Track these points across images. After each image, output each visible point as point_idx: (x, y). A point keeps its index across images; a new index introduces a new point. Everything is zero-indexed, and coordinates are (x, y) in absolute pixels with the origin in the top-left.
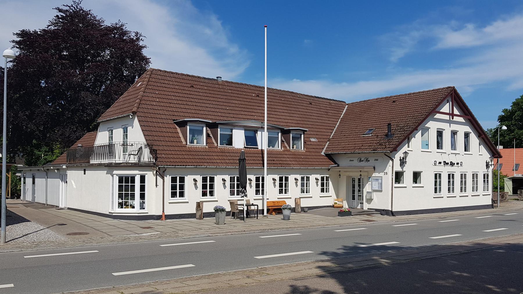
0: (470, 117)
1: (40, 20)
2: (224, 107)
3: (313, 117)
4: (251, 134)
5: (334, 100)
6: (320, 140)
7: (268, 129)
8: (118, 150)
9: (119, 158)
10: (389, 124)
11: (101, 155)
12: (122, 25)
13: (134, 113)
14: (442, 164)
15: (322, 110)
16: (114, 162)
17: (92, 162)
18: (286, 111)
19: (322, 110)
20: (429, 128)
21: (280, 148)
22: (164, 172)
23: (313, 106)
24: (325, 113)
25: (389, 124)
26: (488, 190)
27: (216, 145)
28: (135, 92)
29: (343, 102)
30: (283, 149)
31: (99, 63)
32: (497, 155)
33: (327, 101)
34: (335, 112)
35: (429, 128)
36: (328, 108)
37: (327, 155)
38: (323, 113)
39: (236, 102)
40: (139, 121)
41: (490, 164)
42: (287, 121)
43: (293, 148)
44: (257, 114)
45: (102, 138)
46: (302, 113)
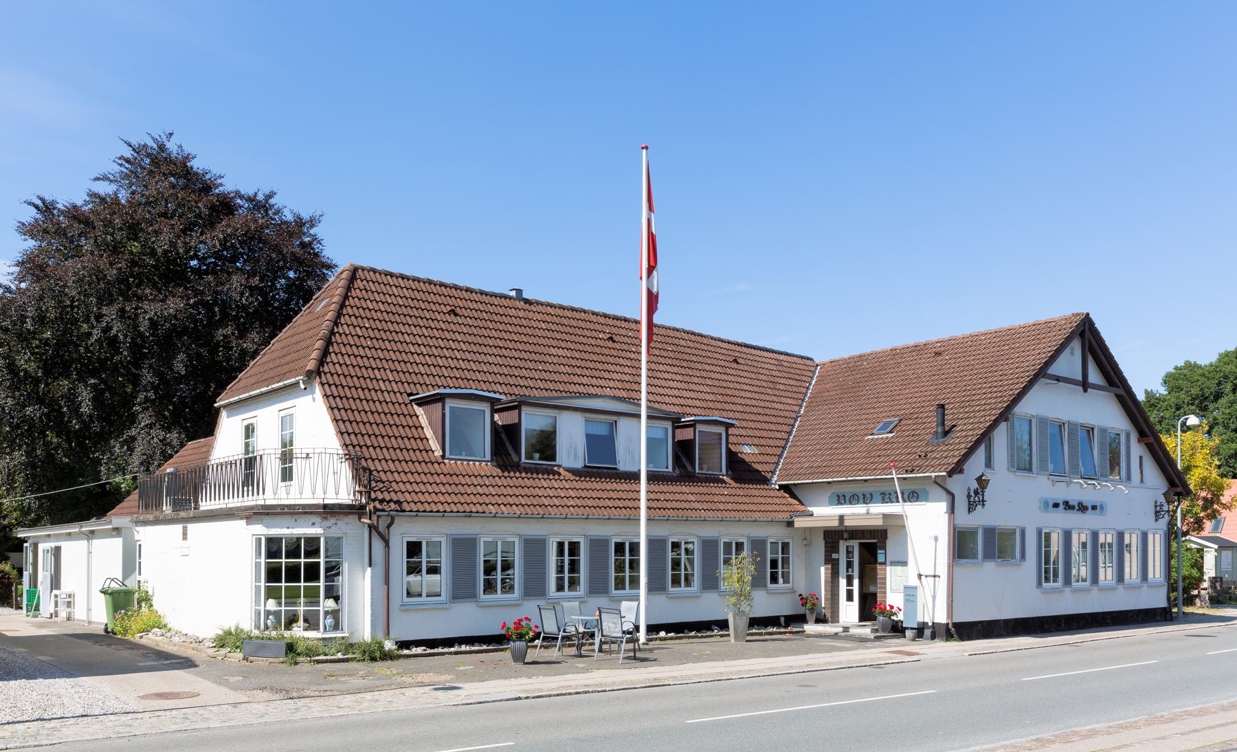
0: (1121, 392)
1: (82, 174)
2: (531, 365)
3: (743, 394)
4: (602, 430)
5: (788, 354)
6: (763, 450)
7: (649, 417)
8: (270, 469)
9: (273, 492)
10: (942, 406)
11: (224, 488)
12: (270, 196)
13: (310, 375)
14: (1062, 507)
15: (761, 377)
16: (262, 503)
17: (206, 505)
18: (679, 377)
19: (761, 377)
20: (1146, 392)
21: (670, 469)
22: (389, 526)
23: (740, 367)
24: (771, 385)
25: (942, 406)
26: (1055, 581)
27: (515, 458)
28: (310, 325)
29: (808, 359)
30: (678, 471)
31: (179, 365)
32: (1179, 490)
33: (771, 355)
34: (792, 382)
35: (1146, 392)
36: (774, 373)
37: (782, 487)
38: (764, 384)
39: (561, 352)
40: (326, 396)
41: (1165, 508)
42: (682, 401)
43: (701, 469)
44: (612, 384)
45: (227, 440)
46: (716, 383)
